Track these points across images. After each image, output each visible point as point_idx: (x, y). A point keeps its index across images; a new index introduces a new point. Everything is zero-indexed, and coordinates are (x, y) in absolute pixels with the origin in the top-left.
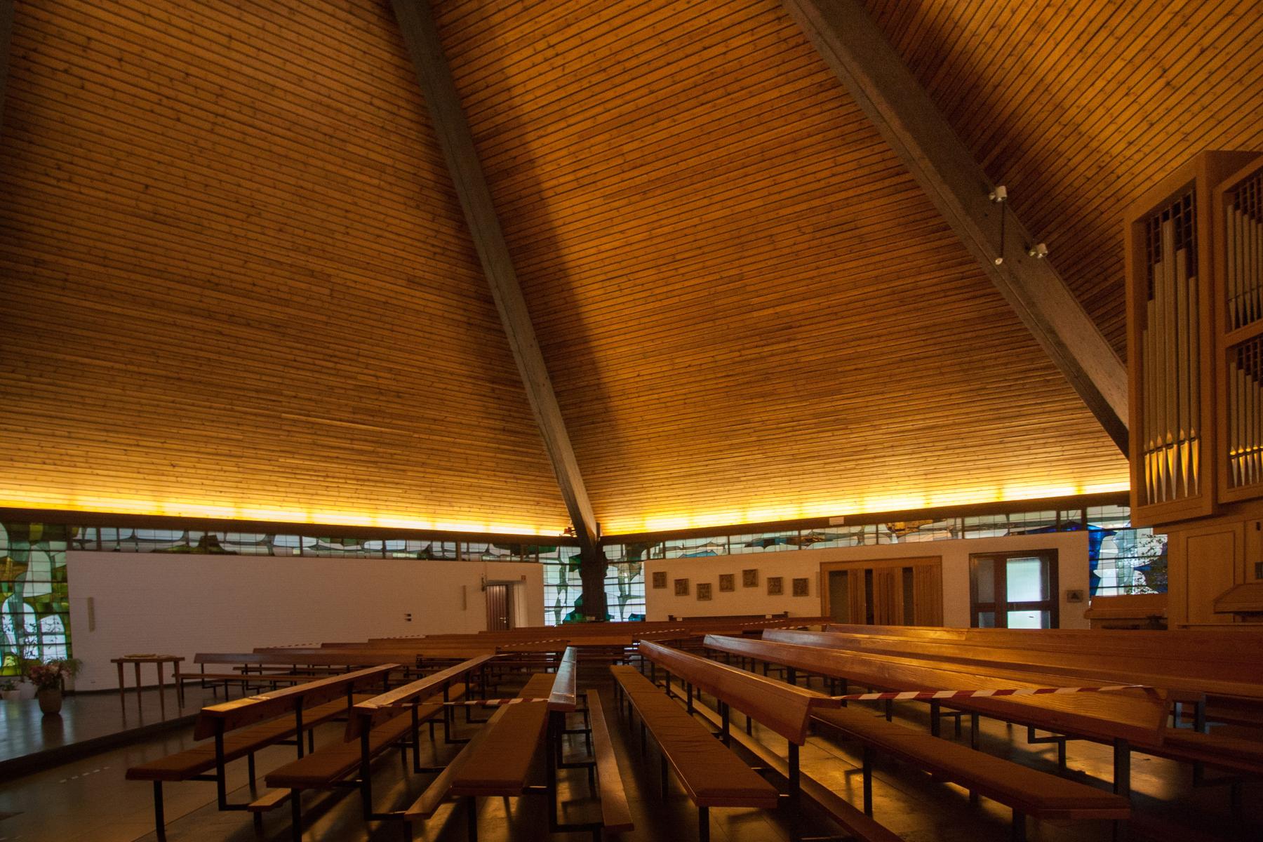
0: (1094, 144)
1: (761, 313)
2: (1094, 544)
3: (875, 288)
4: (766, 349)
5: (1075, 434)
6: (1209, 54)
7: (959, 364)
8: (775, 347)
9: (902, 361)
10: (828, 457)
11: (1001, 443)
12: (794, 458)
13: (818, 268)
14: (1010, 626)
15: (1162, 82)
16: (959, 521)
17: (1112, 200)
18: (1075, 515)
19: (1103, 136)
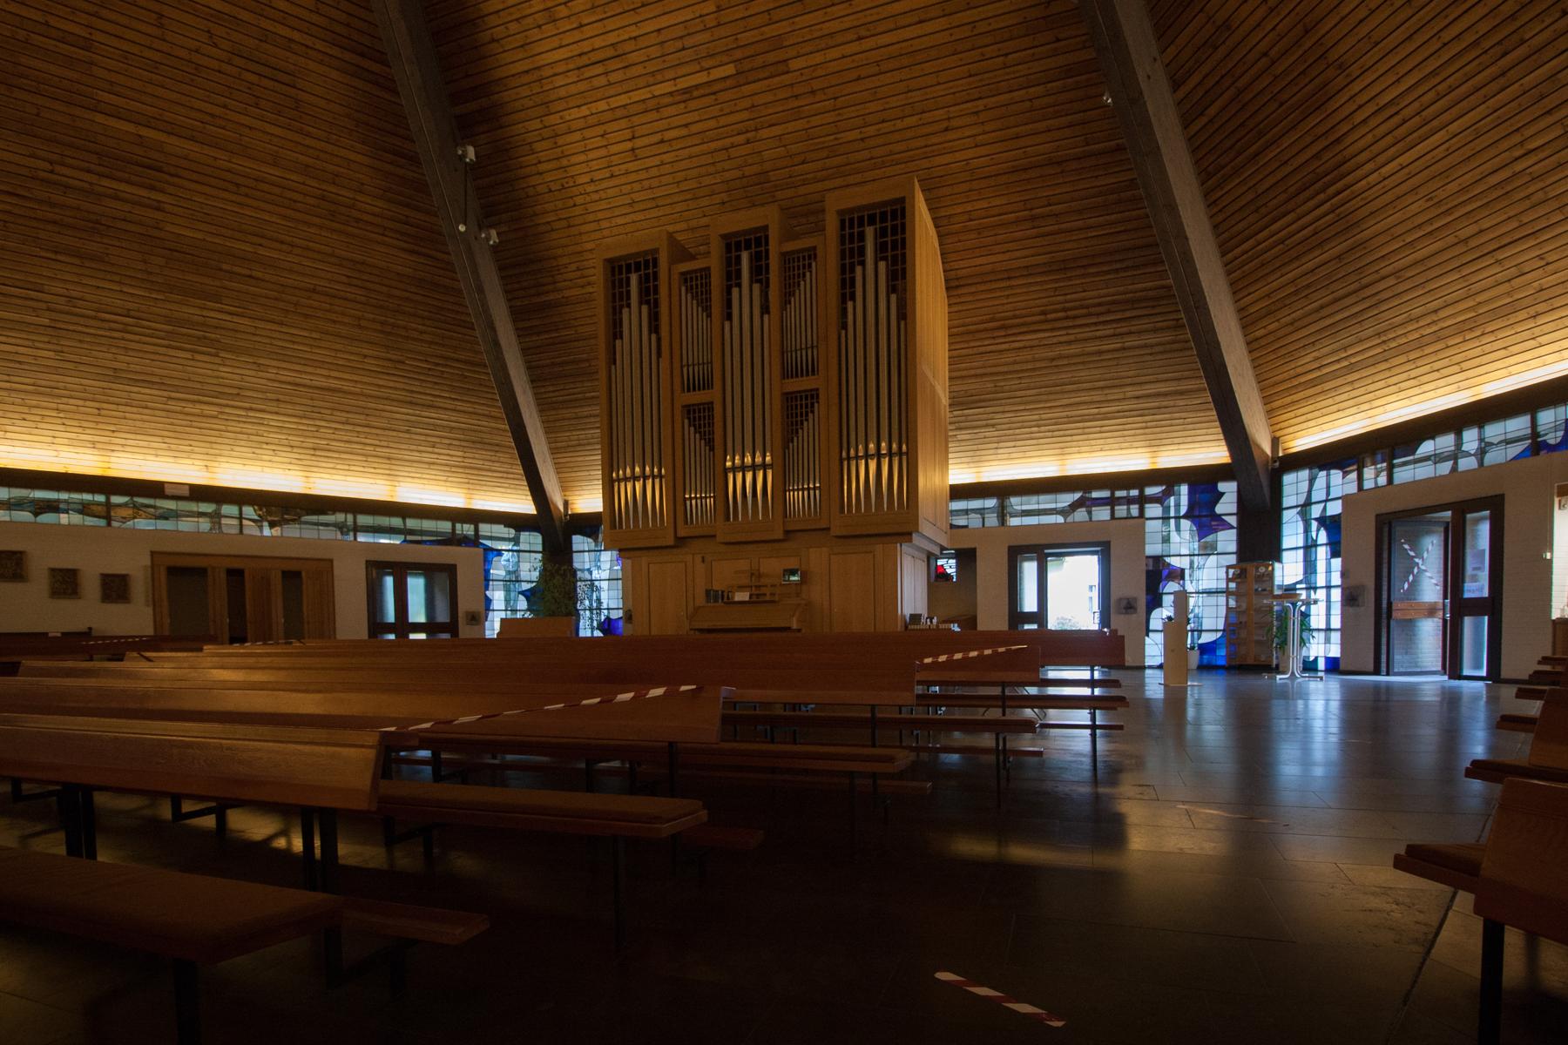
0: (565, 162)
1: (112, 122)
2: (487, 562)
3: (300, 179)
4: (106, 182)
5: (475, 442)
6: (664, 148)
7: (382, 323)
8: (123, 187)
9: (314, 291)
10: (176, 389)
11: (408, 432)
12: (116, 376)
13: (225, 107)
14: (980, 628)
15: (629, 145)
16: (350, 517)
17: (564, 223)
18: (468, 529)
19: (574, 159)
